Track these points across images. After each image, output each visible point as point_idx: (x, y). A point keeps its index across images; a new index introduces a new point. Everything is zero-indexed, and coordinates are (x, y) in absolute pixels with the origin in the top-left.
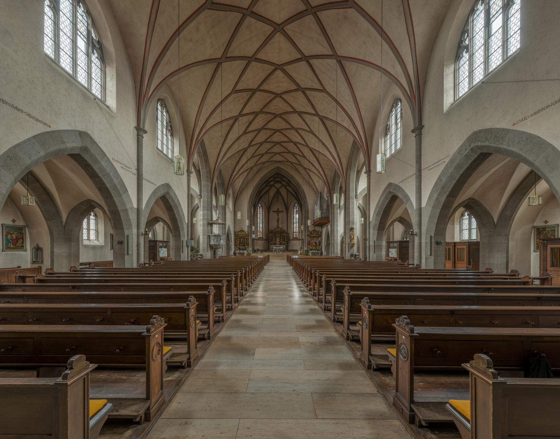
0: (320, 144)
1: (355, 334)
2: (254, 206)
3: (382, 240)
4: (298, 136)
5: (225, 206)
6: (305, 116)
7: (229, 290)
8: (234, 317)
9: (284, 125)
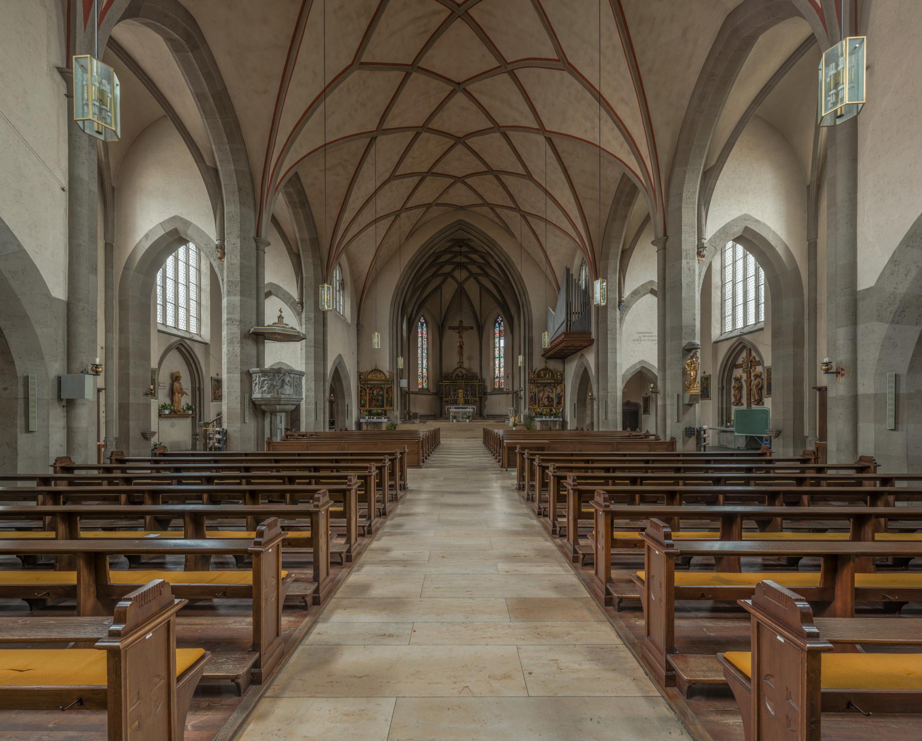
4: (517, 98)
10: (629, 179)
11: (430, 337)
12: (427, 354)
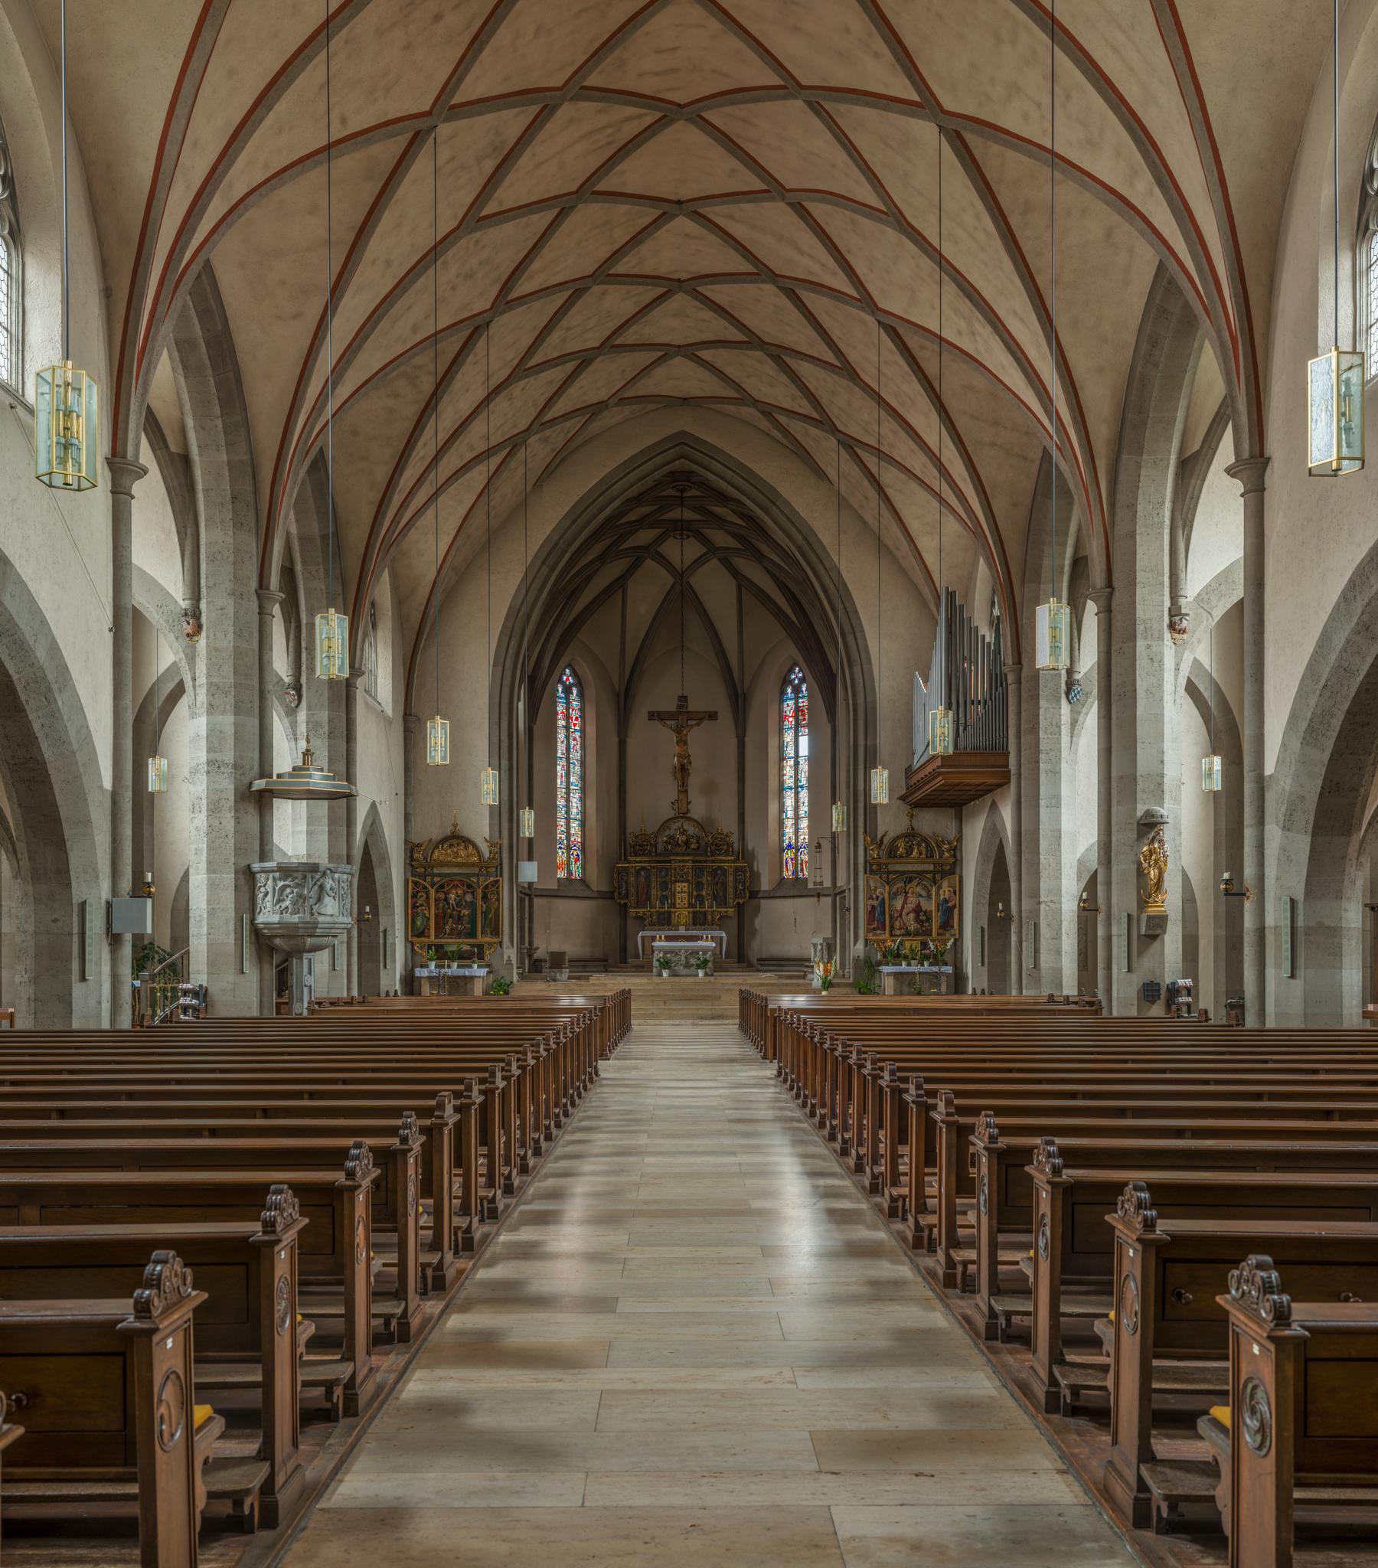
0: (950, 288)
1: (1193, 1485)
2: (528, 680)
3: (1339, 896)
5: (349, 685)
6: (849, 115)
7: (387, 1212)
8: (419, 1385)
9: (718, 171)
10: (1172, 282)
11: (591, 730)
12: (583, 778)
